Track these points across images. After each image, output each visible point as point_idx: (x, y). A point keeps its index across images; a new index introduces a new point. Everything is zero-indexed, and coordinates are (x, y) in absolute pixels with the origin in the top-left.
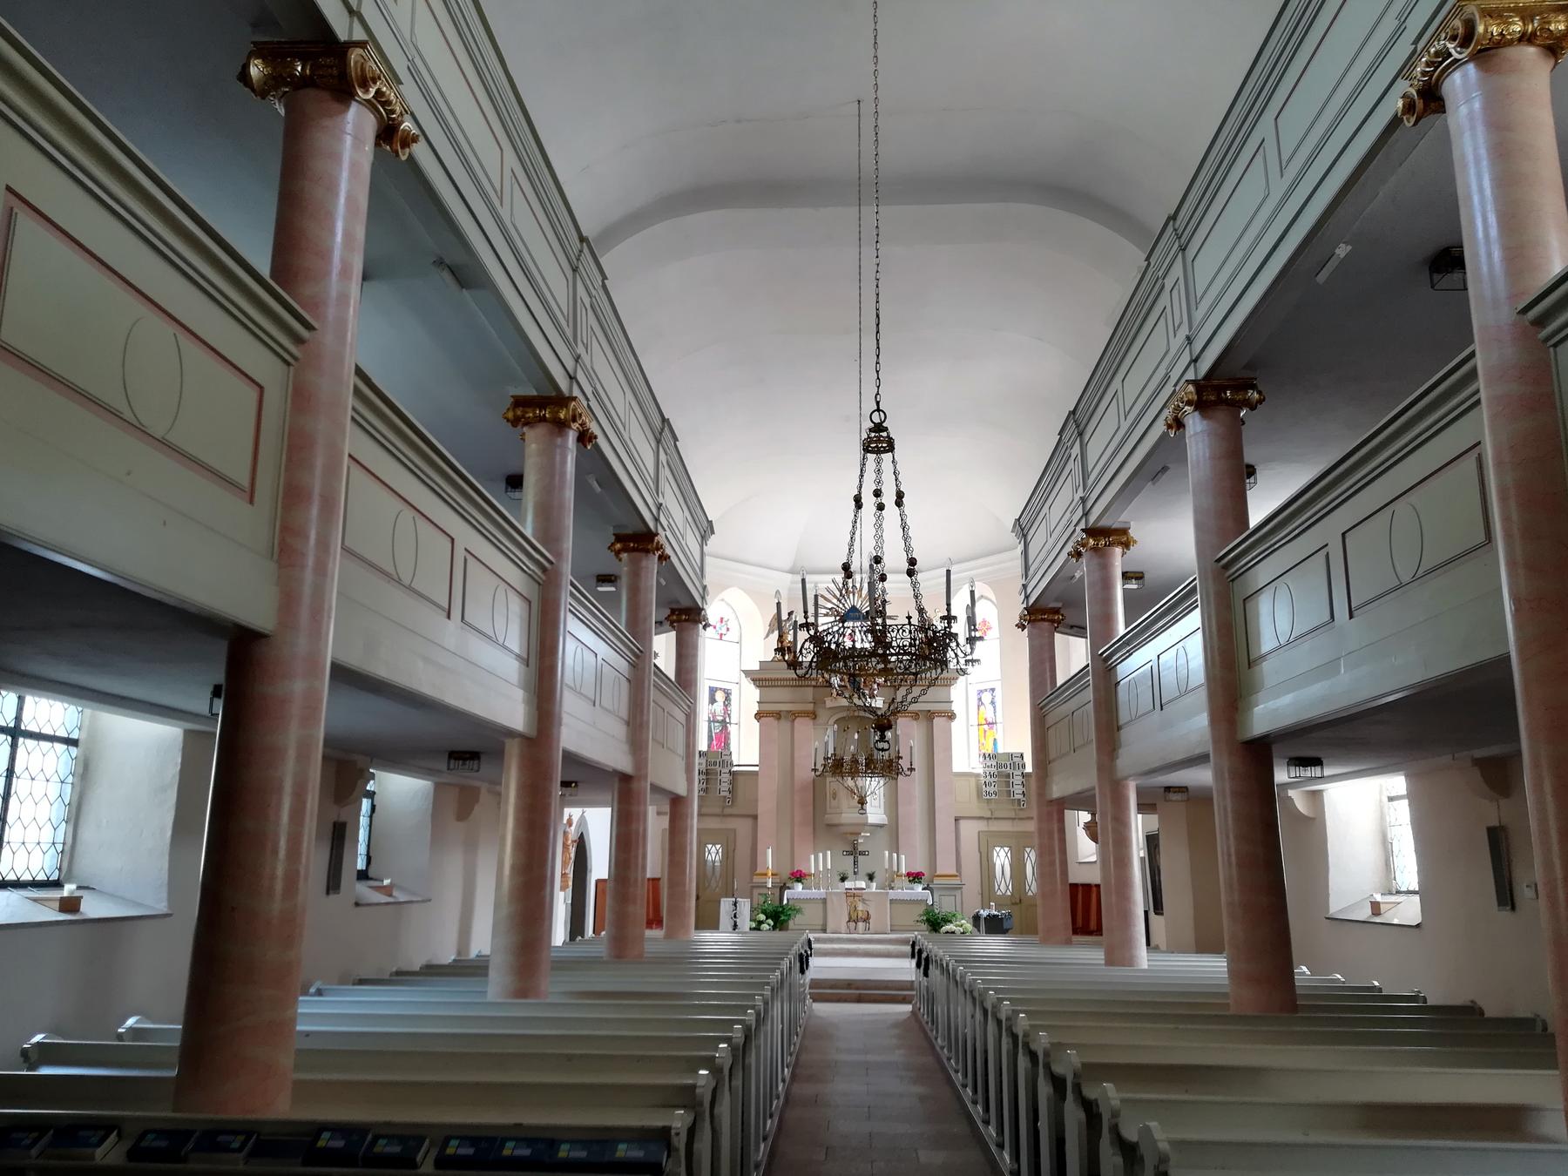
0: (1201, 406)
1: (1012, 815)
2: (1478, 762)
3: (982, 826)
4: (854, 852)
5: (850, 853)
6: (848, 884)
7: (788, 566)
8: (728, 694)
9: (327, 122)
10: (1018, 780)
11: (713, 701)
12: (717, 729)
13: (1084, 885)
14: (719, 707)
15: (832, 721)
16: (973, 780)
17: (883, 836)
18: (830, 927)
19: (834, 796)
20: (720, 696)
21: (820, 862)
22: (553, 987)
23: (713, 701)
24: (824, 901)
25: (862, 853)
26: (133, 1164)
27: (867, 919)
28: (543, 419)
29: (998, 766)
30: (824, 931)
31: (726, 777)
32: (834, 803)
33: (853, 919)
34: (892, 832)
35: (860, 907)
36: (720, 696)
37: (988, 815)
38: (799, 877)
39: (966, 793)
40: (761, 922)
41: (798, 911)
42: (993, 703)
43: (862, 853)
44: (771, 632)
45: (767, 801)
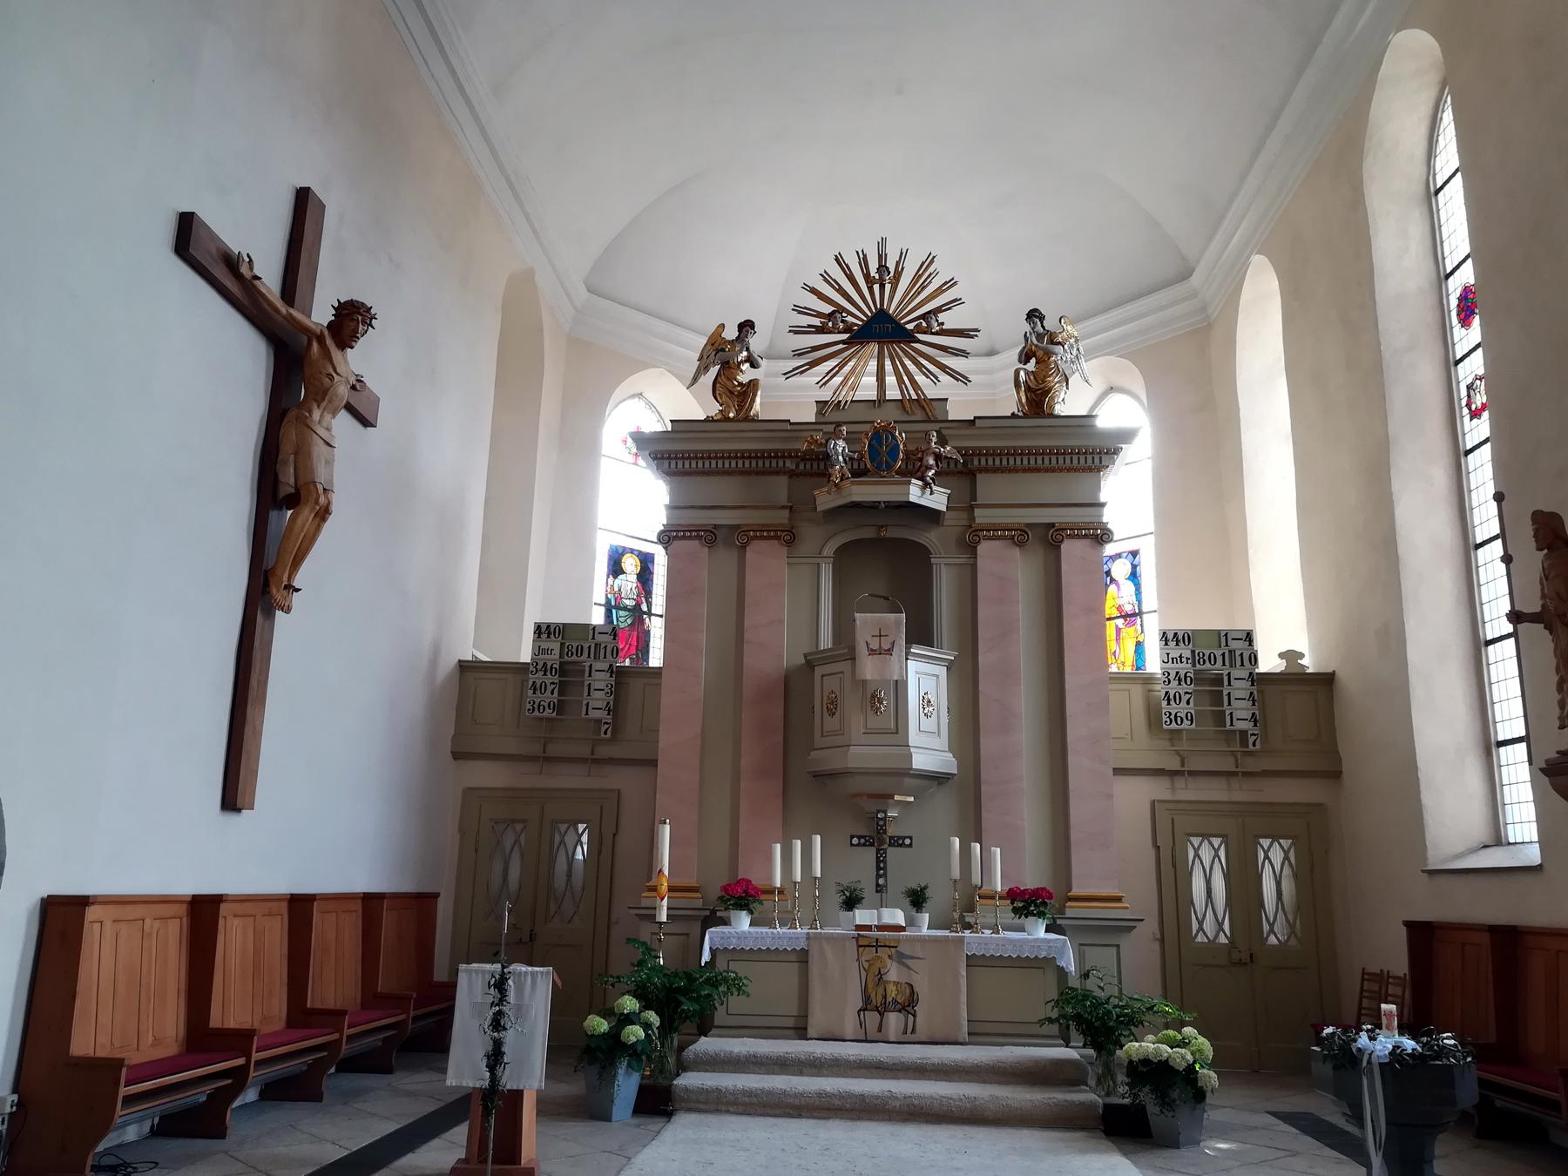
1: (1227, 764)
3: (1156, 789)
4: (878, 838)
5: (867, 842)
6: (862, 916)
10: (1240, 689)
13: (1496, 931)
14: (628, 582)
15: (829, 550)
16: (1137, 691)
17: (943, 806)
18: (816, 1023)
19: (832, 707)
20: (631, 564)
21: (794, 861)
23: (616, 569)
24: (803, 957)
25: (897, 842)
26: (754, 930)
27: (908, 1006)
29: (1194, 658)
30: (801, 1032)
31: (601, 680)
32: (831, 723)
33: (875, 1004)
34: (966, 792)
35: (893, 973)
37: (1173, 764)
38: (743, 896)
39: (1125, 711)
40: (628, 1019)
41: (736, 985)
42: (1134, 576)
43: (897, 842)
44: (703, 369)
45: (678, 730)
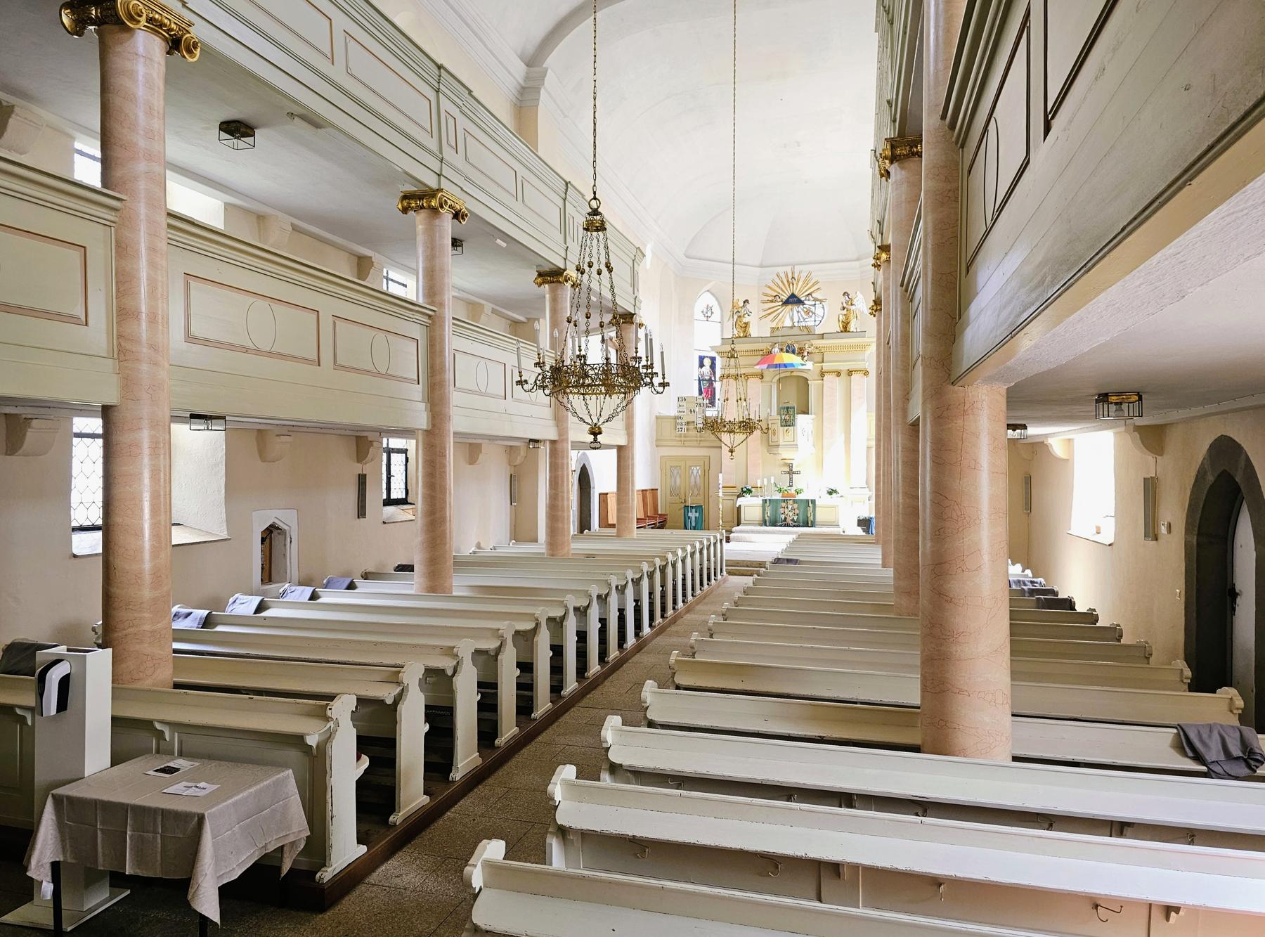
0: (893, 159)
2: (1138, 429)
7: (758, 263)
8: (713, 359)
9: (119, 49)
11: (701, 365)
12: (705, 385)
14: (706, 369)
20: (707, 362)
22: (460, 584)
23: (701, 365)
28: (422, 207)
36: (707, 362)
